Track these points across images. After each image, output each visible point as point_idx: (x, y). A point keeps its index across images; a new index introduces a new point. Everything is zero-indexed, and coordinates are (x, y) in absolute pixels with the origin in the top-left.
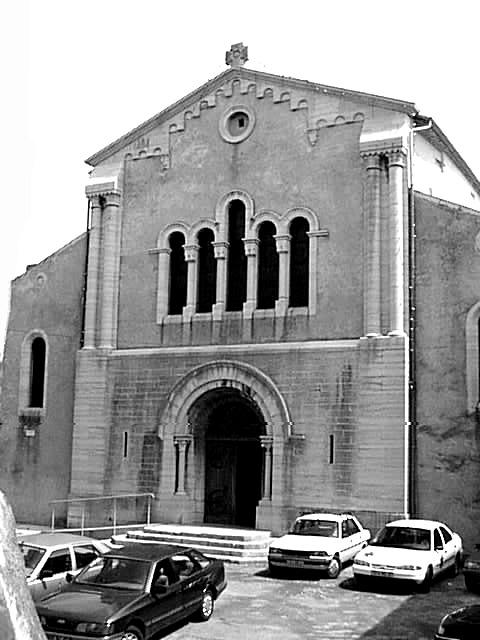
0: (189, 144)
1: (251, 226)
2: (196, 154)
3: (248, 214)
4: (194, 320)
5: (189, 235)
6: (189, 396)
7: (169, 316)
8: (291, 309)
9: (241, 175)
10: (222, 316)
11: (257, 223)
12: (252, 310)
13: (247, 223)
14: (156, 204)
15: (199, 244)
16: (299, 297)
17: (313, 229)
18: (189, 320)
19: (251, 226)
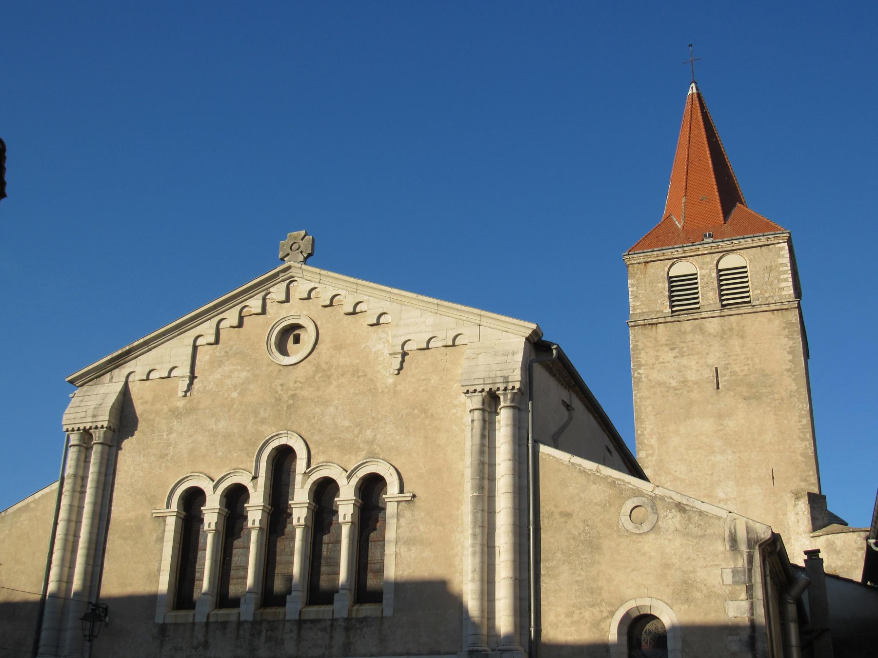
0: (220, 364)
1: (303, 483)
2: (229, 377)
3: (300, 465)
4: (212, 619)
5: (255, 487)
6: (689, 314)
7: (174, 613)
8: (356, 607)
9: (346, 426)
10: (254, 614)
11: (315, 477)
12: (299, 606)
13: (299, 478)
14: (169, 445)
15: (184, 511)
16: (745, 267)
17: (392, 489)
18: (204, 620)
19: (303, 483)
